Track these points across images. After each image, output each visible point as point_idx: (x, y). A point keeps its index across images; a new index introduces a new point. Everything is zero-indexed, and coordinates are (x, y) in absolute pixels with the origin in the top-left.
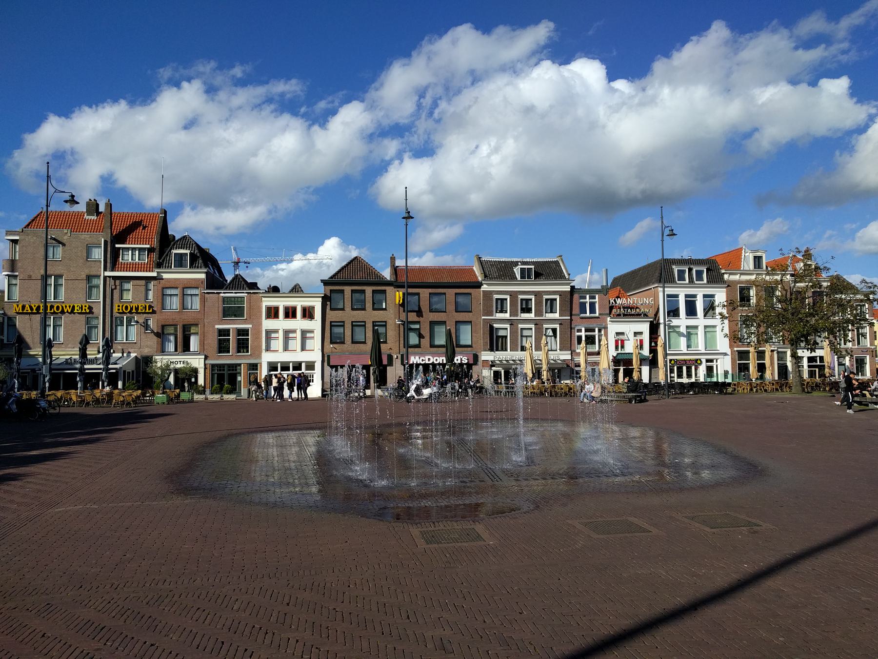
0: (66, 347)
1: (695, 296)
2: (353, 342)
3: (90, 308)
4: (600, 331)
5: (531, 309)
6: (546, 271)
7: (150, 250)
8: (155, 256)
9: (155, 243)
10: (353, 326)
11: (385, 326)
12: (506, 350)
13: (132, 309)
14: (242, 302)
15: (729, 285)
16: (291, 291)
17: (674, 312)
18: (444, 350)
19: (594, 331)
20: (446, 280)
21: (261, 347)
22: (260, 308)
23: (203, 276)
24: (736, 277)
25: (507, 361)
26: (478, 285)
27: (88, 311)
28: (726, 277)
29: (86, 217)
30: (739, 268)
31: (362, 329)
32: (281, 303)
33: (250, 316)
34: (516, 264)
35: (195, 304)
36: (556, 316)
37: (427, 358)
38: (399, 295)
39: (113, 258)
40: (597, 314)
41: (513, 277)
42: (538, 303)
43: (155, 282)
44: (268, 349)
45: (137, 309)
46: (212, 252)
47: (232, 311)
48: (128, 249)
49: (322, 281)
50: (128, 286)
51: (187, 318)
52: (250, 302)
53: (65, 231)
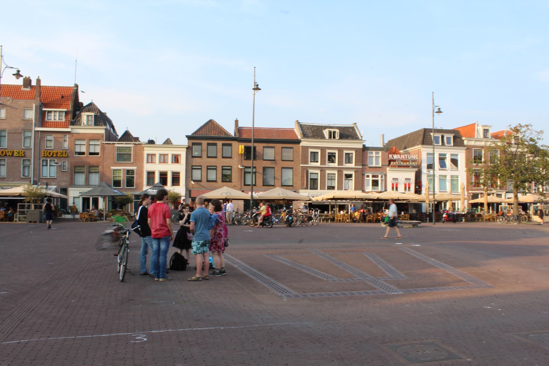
0: (8, 181)
1: (445, 155)
6: (348, 133)
7: (67, 113)
8: (70, 117)
9: (70, 108)
10: (208, 169)
11: (231, 170)
12: (317, 189)
13: (53, 154)
14: (130, 150)
15: (469, 149)
16: (165, 143)
19: (378, 176)
21: (142, 183)
22: (142, 155)
23: (103, 132)
24: (472, 143)
26: (298, 142)
27: (23, 155)
28: (466, 142)
29: (23, 89)
30: (474, 136)
32: (157, 152)
33: (135, 160)
34: (325, 127)
36: (353, 165)
38: (241, 148)
40: (380, 165)
41: (323, 137)
43: (70, 135)
45: (57, 154)
46: (109, 115)
48: (51, 112)
49: (187, 136)
50: (49, 138)
52: (135, 150)
53: (8, 98)
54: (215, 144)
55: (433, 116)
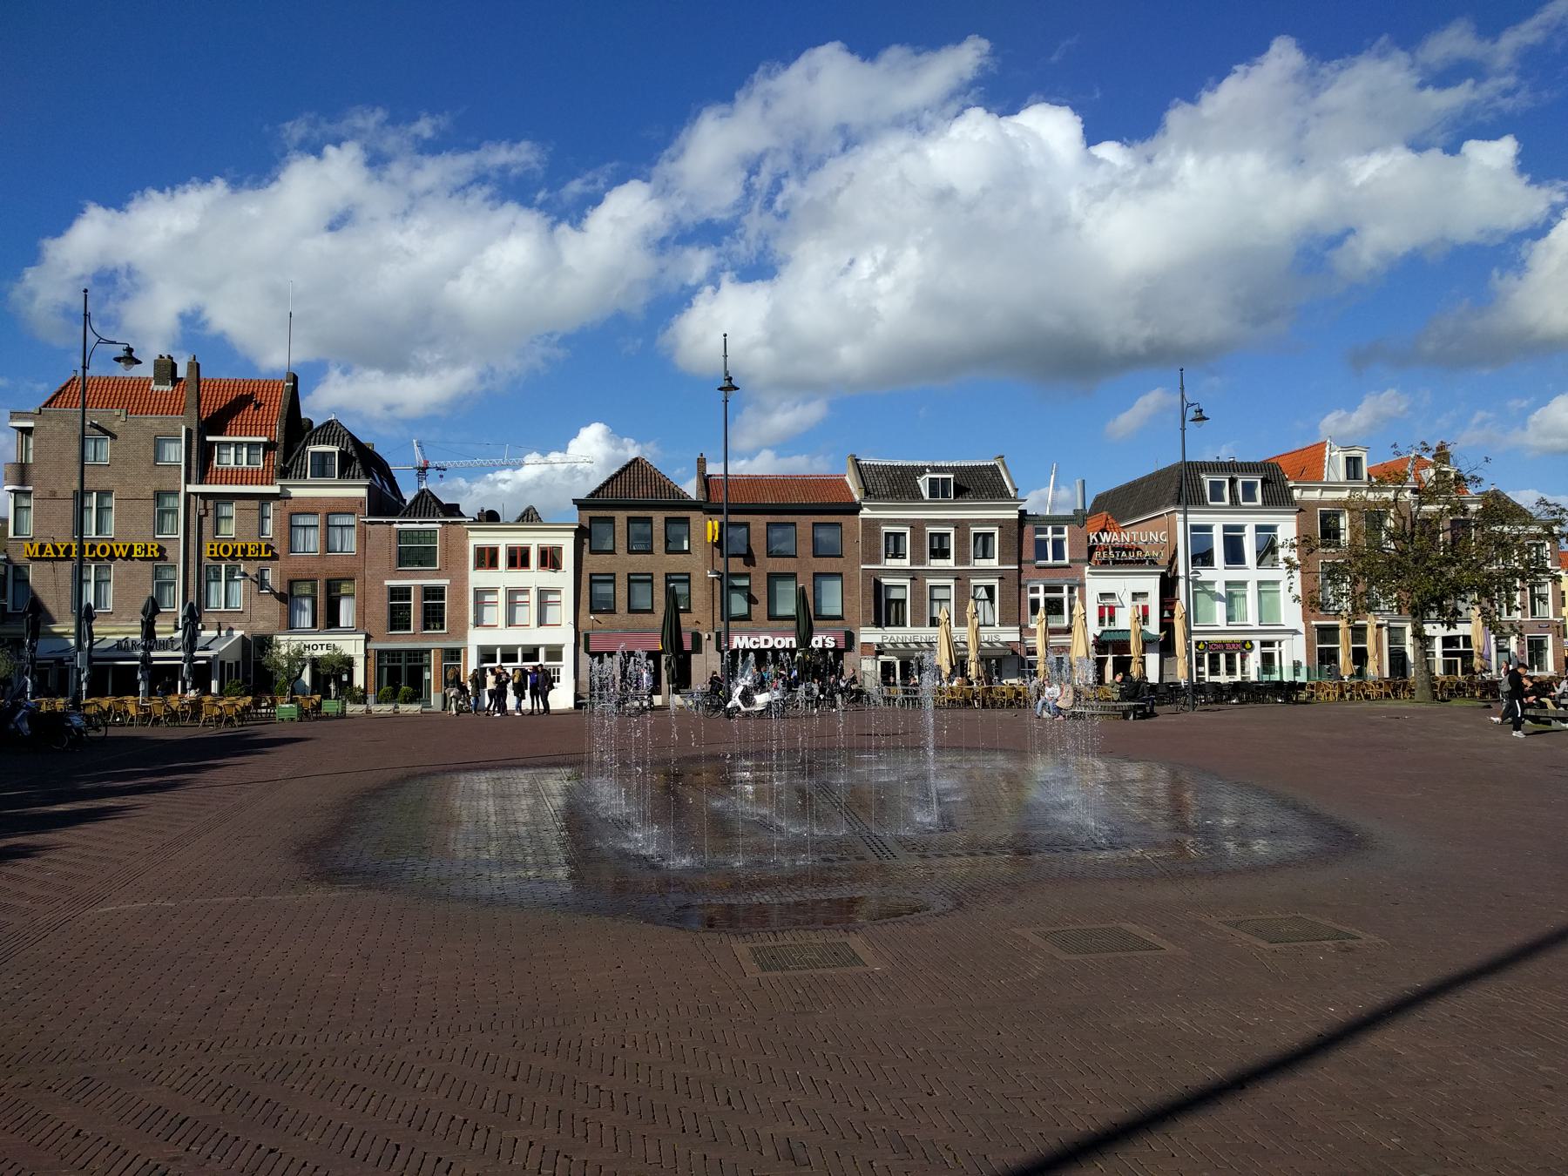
0: (118, 620)
1: (1241, 528)
2: (630, 611)
3: (161, 550)
4: (1071, 590)
5: (948, 552)
6: (975, 484)
7: (269, 447)
8: (276, 456)
9: (277, 434)
10: (630, 581)
11: (688, 581)
12: (904, 625)
13: (235, 551)
14: (433, 538)
15: (1302, 509)
16: (520, 519)
17: (1203, 557)
18: (793, 624)
19: (1060, 590)
20: (797, 499)
21: (465, 618)
22: (464, 549)
23: (363, 493)
24: (1315, 495)
25: (906, 644)
26: (854, 509)
27: (157, 555)
28: (1296, 494)
29: (154, 387)
30: (1319, 478)
31: (647, 586)
32: (502, 541)
33: (446, 563)
34: (921, 471)
35: (349, 542)
36: (994, 563)
37: (762, 638)
38: (712, 526)
39: (202, 461)
40: (1066, 561)
41: (917, 495)
42: (962, 541)
43: (278, 503)
44: (478, 623)
45: (245, 551)
46: (379, 450)
47: (415, 554)
48: (229, 444)
49: (575, 501)
50: (229, 510)
51: (334, 568)
52: (446, 539)
53: (117, 412)
54: (611, 520)
55: (1183, 429)
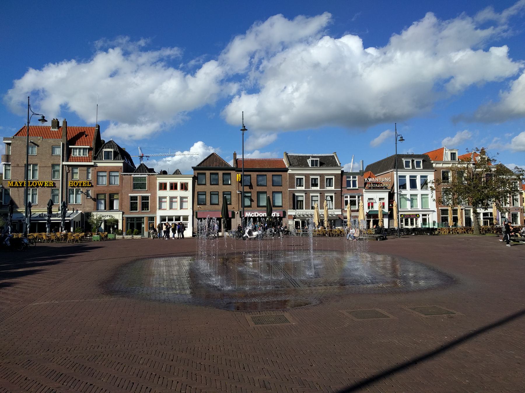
0: (39, 207)
1: (415, 177)
2: (211, 204)
3: (54, 184)
4: (359, 197)
5: (317, 184)
6: (327, 162)
7: (90, 149)
8: (92, 152)
9: (93, 145)
10: (211, 194)
11: (230, 194)
12: (303, 209)
13: (79, 184)
14: (145, 180)
15: (436, 170)
16: (174, 174)
17: (403, 186)
18: (265, 208)
19: (355, 197)
20: (267, 167)
21: (156, 207)
22: (155, 184)
23: (121, 165)
25: (303, 215)
26: (286, 170)
27: (52, 185)
29: (52, 129)
30: (442, 160)
31: (217, 196)
32: (168, 181)
33: (149, 188)
34: (309, 157)
35: (117, 181)
36: (333, 188)
37: (255, 213)
38: (238, 176)
39: (68, 154)
40: (357, 188)
41: (307, 165)
42: (322, 181)
43: (93, 168)
44: (160, 208)
45: (82, 184)
46: (127, 150)
47: (139, 185)
48: (77, 148)
49: (193, 168)
50: (77, 170)
51: (112, 190)
52: (149, 180)
53: (39, 138)
54: (205, 174)
55: (396, 143)
